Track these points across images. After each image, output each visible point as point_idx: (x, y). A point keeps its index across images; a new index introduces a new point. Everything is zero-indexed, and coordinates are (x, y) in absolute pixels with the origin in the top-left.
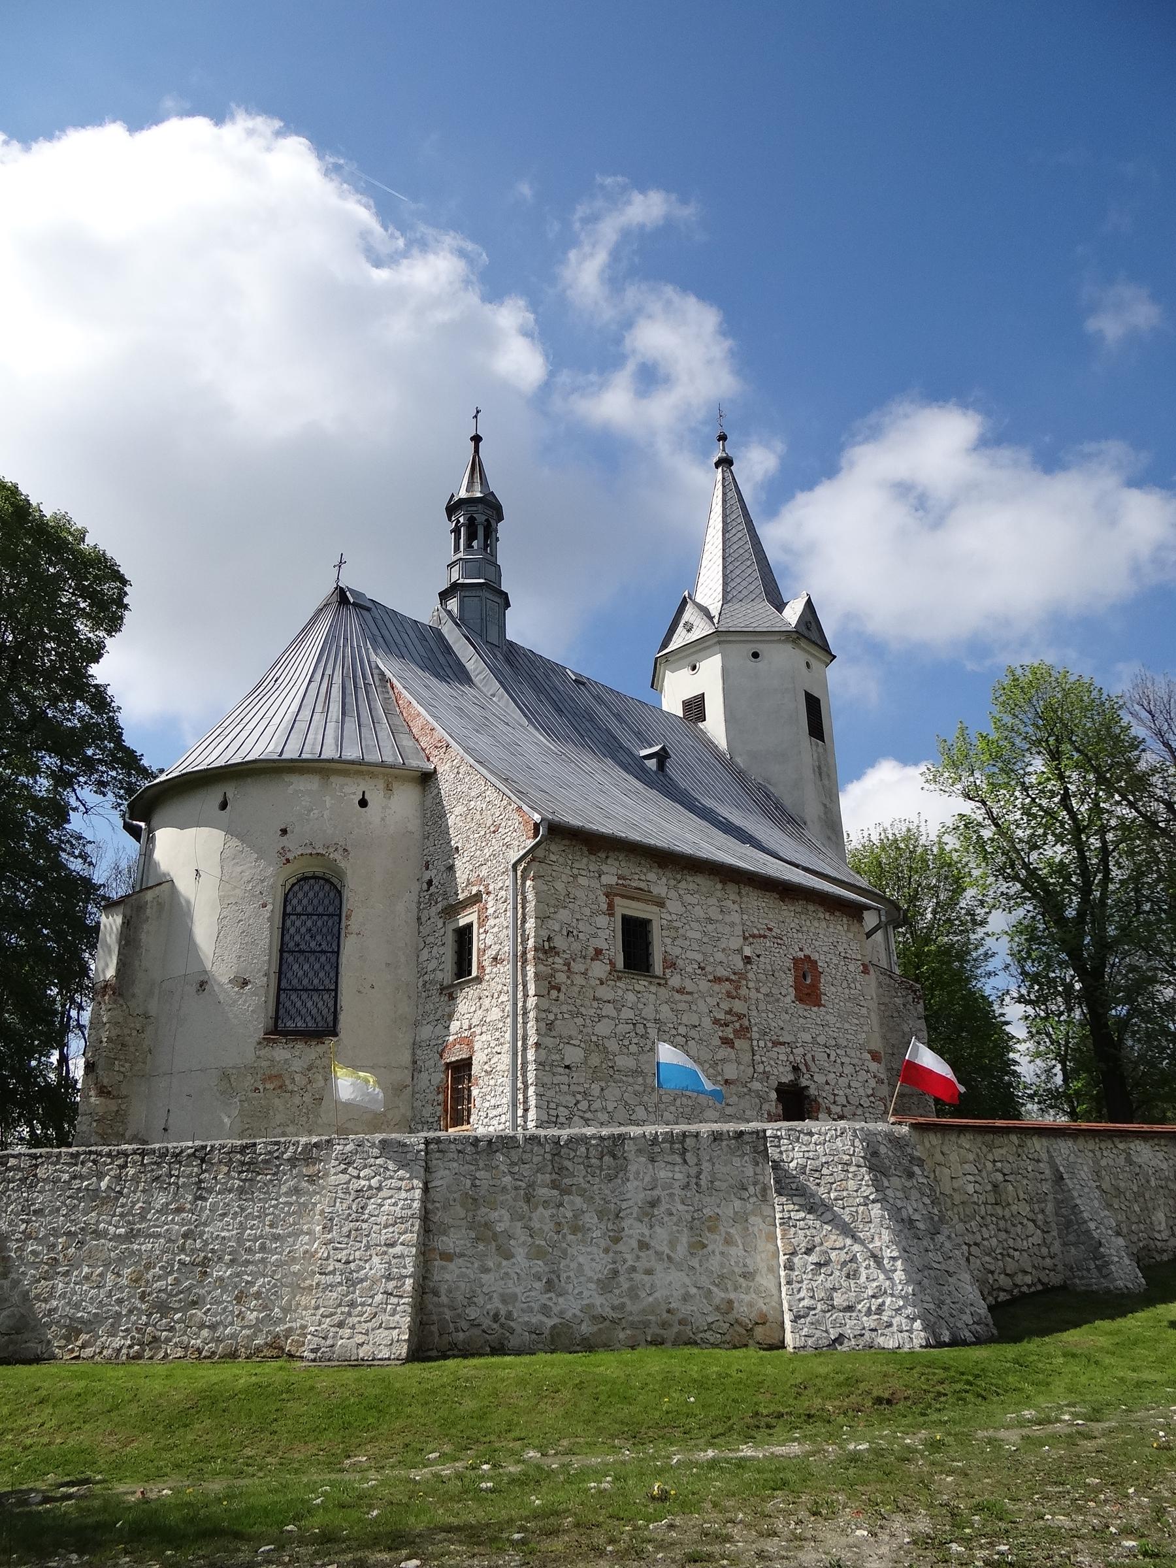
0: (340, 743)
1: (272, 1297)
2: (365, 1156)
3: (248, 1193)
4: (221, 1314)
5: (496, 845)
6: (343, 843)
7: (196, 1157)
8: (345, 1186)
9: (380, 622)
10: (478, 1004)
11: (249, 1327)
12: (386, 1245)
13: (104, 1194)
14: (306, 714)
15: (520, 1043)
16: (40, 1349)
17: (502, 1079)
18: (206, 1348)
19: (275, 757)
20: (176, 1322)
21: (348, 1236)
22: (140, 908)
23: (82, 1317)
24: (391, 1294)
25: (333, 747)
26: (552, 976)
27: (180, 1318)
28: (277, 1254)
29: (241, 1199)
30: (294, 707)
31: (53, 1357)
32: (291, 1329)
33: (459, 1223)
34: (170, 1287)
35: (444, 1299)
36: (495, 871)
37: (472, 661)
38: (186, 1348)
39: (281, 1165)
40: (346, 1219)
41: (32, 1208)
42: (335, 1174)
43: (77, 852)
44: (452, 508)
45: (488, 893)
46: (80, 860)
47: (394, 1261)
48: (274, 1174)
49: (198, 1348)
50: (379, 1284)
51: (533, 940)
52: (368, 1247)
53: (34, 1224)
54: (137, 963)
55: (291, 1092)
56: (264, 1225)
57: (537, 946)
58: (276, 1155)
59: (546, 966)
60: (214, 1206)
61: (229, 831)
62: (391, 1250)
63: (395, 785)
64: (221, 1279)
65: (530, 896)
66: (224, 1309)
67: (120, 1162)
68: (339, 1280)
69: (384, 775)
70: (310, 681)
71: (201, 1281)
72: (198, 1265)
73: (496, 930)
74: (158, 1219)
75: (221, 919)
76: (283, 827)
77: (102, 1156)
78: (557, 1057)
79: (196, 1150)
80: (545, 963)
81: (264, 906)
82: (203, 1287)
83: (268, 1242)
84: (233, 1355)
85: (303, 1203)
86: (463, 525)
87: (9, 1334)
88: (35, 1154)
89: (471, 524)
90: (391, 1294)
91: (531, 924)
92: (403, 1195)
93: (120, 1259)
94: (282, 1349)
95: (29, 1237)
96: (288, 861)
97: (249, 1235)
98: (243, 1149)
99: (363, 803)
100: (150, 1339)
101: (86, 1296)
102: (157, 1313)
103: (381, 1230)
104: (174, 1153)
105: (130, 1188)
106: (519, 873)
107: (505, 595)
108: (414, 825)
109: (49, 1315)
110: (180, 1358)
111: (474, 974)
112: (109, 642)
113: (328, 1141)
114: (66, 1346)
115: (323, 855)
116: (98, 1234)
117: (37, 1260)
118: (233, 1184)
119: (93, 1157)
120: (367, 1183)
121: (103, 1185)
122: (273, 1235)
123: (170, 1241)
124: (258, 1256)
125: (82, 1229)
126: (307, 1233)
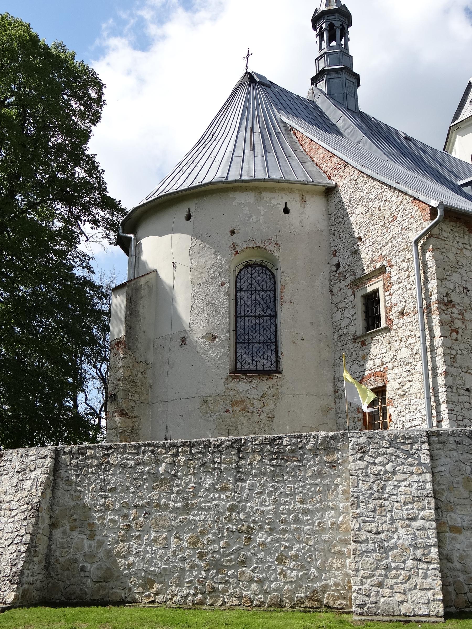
0: (267, 168)
1: (308, 560)
2: (377, 446)
3: (278, 476)
4: (266, 572)
5: (395, 230)
6: (275, 239)
7: (233, 448)
8: (364, 471)
9: (277, 95)
10: (388, 347)
11: (291, 583)
12: (408, 519)
13: (162, 477)
14: (239, 152)
15: (430, 372)
16: (123, 594)
17: (415, 400)
18: (257, 598)
19: (223, 179)
20: (229, 577)
21: (374, 511)
22: (137, 289)
23: (154, 571)
24: (420, 560)
25: (263, 172)
26: (452, 322)
27: (233, 574)
28: (308, 525)
29: (273, 481)
30: (231, 148)
31: (134, 601)
32: (326, 585)
33: (463, 502)
34: (222, 550)
35: (457, 565)
36: (396, 249)
37: (341, 121)
38: (240, 598)
39: (305, 454)
40: (370, 497)
41: (108, 487)
42: (354, 461)
43: (84, 265)
44: (316, 20)
45: (391, 266)
46: (86, 270)
47: (418, 533)
48: (299, 461)
49: (250, 598)
50: (408, 552)
51: (436, 295)
52: (393, 521)
53: (111, 499)
54: (138, 326)
55: (252, 413)
56: (295, 502)
57: (440, 300)
58: (300, 445)
59: (447, 314)
60: (252, 486)
61: (194, 235)
62: (413, 524)
63: (308, 198)
64: (264, 544)
65: (431, 263)
66: (269, 568)
67: (173, 451)
68: (372, 547)
69: (300, 190)
70: (238, 132)
71: (247, 545)
72: (243, 532)
73: (400, 291)
74: (207, 496)
75: (193, 295)
76: (232, 229)
77: (158, 447)
78: (460, 382)
79: (233, 443)
80: (446, 312)
81: (223, 284)
82: (249, 550)
83: (300, 515)
84: (279, 605)
85: (327, 484)
86: (325, 29)
87: (99, 582)
88: (106, 446)
89: (331, 28)
90: (420, 560)
91: (433, 284)
92: (416, 478)
93: (180, 527)
94: (320, 601)
95: (108, 509)
96: (237, 252)
97: (284, 509)
98: (272, 441)
99: (286, 211)
100: (210, 590)
101: (156, 555)
102: (213, 569)
103: (402, 507)
104: (215, 445)
105: (182, 472)
106: (419, 248)
107: (357, 77)
108: (323, 225)
109: (128, 569)
110: (236, 605)
111: (383, 324)
112: (93, 128)
113: (343, 435)
114: (143, 592)
115: (261, 248)
116: (160, 507)
117: (115, 526)
118: (266, 470)
119: (151, 448)
120: (382, 468)
121: (161, 469)
122: (304, 510)
123: (218, 513)
124: (293, 526)
125: (148, 503)
126: (332, 509)
